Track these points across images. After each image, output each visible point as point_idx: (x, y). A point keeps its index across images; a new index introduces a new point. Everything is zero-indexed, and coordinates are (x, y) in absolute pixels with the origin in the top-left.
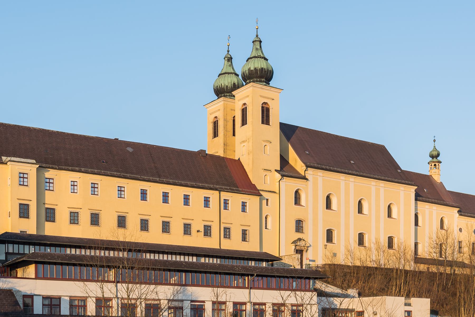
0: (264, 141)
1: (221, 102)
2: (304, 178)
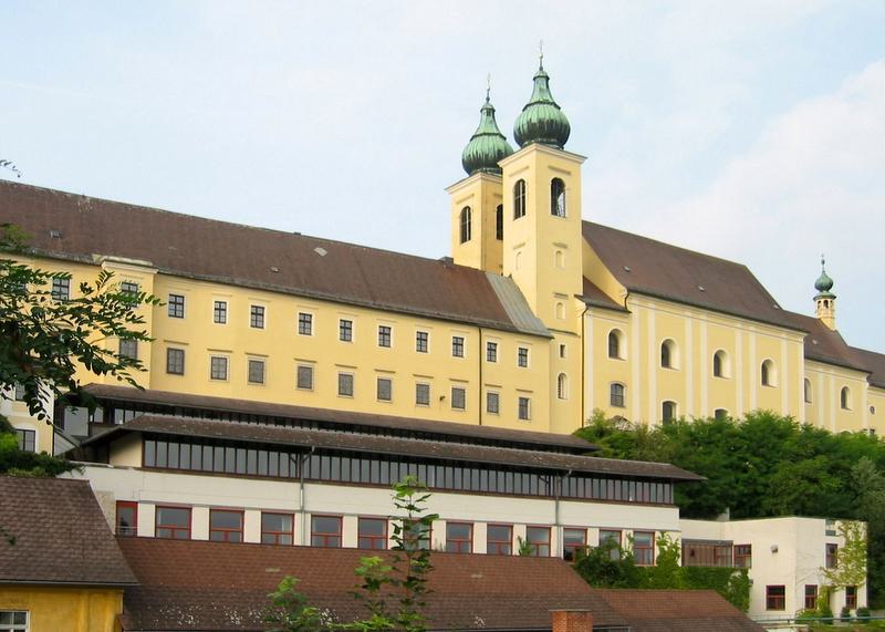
0: (556, 245)
1: (477, 182)
2: (625, 311)
